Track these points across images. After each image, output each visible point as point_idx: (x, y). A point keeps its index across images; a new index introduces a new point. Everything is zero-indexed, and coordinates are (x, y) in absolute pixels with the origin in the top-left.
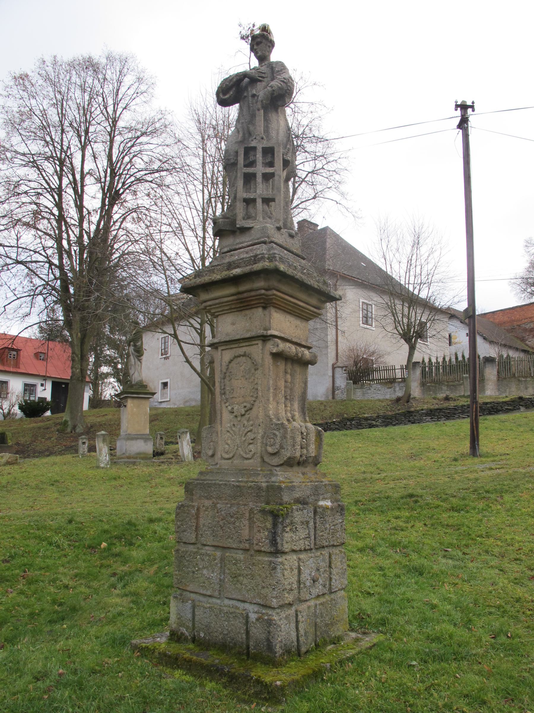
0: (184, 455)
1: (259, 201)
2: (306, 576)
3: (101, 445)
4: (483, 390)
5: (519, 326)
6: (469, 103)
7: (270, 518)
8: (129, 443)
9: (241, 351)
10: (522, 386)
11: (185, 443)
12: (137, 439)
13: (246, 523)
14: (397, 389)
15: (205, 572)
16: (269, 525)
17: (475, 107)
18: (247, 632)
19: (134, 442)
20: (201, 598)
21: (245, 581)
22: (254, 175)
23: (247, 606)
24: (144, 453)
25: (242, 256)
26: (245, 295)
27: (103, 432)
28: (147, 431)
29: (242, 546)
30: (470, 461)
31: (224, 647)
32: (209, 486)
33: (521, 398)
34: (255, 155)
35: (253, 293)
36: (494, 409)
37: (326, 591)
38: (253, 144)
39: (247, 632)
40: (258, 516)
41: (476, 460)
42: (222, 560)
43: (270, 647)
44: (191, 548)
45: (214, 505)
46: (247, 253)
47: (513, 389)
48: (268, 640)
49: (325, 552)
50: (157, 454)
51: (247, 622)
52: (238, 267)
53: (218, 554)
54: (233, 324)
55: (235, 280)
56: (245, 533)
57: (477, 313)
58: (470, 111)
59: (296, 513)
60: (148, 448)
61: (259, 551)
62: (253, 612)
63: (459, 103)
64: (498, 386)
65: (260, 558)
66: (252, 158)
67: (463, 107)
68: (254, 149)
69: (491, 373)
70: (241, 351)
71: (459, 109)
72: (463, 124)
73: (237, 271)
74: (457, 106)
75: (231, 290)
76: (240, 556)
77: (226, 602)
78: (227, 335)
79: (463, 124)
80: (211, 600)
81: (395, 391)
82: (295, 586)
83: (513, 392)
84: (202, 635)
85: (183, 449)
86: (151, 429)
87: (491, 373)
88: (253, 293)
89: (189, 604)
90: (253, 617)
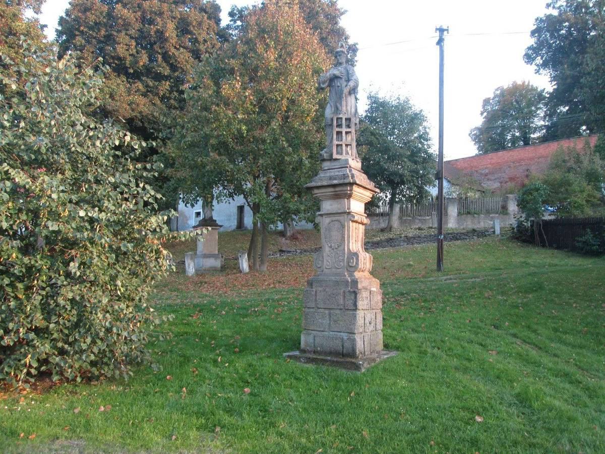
0: (243, 269)
1: (344, 146)
2: (367, 322)
3: (190, 261)
4: (447, 223)
5: (477, 171)
6: (445, 27)
7: (353, 295)
8: (205, 260)
9: (334, 218)
10: (476, 221)
11: (244, 261)
12: (210, 257)
13: (342, 297)
14: (381, 221)
15: (320, 320)
16: (353, 298)
17: (449, 31)
18: (343, 346)
19: (208, 259)
20: (318, 333)
21: (341, 323)
22: (341, 132)
23: (342, 334)
24: (215, 267)
25: (338, 173)
26: (338, 192)
27: (191, 253)
28: (217, 252)
29: (339, 308)
30: (436, 274)
31: (330, 353)
32: (321, 281)
33: (474, 230)
34: (342, 122)
35: (342, 192)
36: (455, 236)
37: (374, 329)
38: (341, 116)
39: (343, 346)
40: (347, 294)
41: (440, 274)
42: (330, 314)
43: (354, 350)
44: (312, 310)
45: (325, 290)
46: (339, 172)
47: (469, 223)
48: (353, 348)
49: (374, 311)
50: (223, 268)
51: (342, 341)
52: (335, 179)
53: (327, 312)
54: (331, 205)
55: (334, 186)
56: (341, 302)
57: (445, 160)
58: (445, 33)
59: (363, 293)
60: (218, 263)
61: (348, 309)
62: (345, 336)
63: (438, 27)
64: (458, 220)
65: (348, 312)
66: (340, 123)
67: (441, 31)
68: (341, 118)
69: (453, 211)
70: (334, 218)
71: (438, 31)
72: (440, 42)
73: (335, 182)
74: (437, 29)
75: (332, 189)
76: (338, 312)
77: (331, 333)
78: (328, 210)
79: (440, 42)
80: (323, 333)
81: (379, 222)
82: (363, 325)
83: (469, 224)
84: (319, 349)
85: (242, 265)
86: (219, 249)
87: (453, 211)
88: (342, 192)
89: (312, 336)
90: (345, 338)
